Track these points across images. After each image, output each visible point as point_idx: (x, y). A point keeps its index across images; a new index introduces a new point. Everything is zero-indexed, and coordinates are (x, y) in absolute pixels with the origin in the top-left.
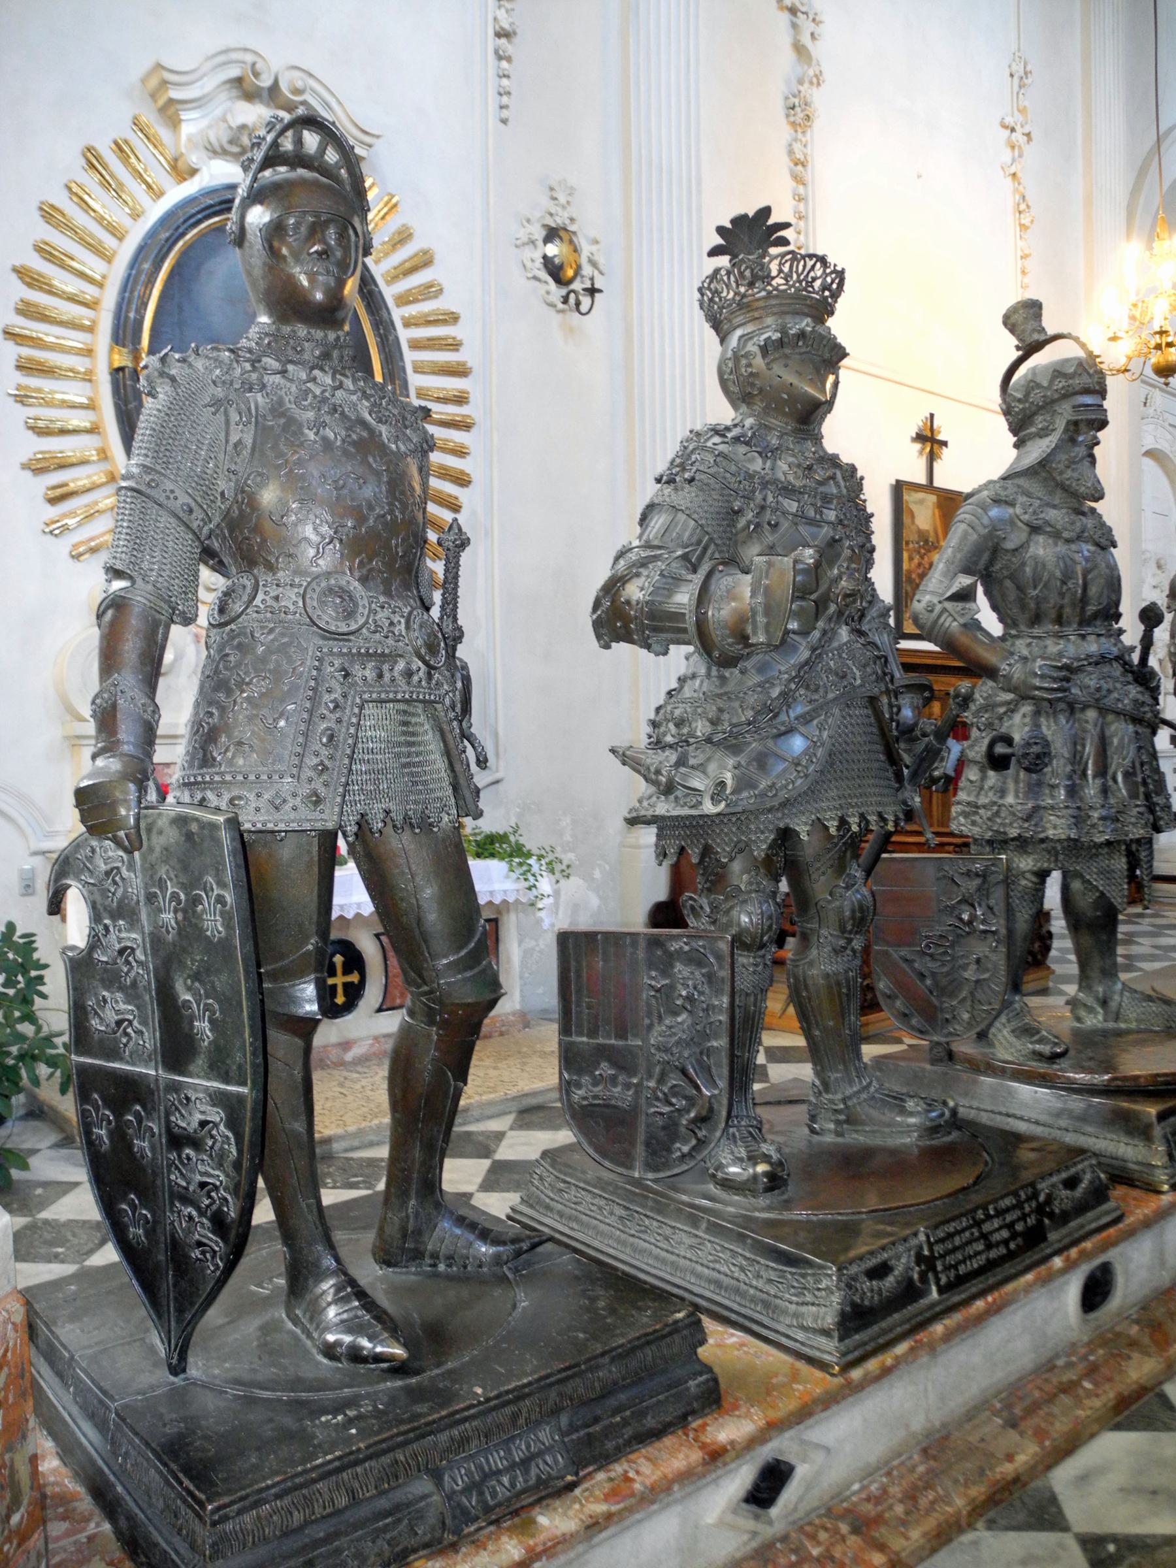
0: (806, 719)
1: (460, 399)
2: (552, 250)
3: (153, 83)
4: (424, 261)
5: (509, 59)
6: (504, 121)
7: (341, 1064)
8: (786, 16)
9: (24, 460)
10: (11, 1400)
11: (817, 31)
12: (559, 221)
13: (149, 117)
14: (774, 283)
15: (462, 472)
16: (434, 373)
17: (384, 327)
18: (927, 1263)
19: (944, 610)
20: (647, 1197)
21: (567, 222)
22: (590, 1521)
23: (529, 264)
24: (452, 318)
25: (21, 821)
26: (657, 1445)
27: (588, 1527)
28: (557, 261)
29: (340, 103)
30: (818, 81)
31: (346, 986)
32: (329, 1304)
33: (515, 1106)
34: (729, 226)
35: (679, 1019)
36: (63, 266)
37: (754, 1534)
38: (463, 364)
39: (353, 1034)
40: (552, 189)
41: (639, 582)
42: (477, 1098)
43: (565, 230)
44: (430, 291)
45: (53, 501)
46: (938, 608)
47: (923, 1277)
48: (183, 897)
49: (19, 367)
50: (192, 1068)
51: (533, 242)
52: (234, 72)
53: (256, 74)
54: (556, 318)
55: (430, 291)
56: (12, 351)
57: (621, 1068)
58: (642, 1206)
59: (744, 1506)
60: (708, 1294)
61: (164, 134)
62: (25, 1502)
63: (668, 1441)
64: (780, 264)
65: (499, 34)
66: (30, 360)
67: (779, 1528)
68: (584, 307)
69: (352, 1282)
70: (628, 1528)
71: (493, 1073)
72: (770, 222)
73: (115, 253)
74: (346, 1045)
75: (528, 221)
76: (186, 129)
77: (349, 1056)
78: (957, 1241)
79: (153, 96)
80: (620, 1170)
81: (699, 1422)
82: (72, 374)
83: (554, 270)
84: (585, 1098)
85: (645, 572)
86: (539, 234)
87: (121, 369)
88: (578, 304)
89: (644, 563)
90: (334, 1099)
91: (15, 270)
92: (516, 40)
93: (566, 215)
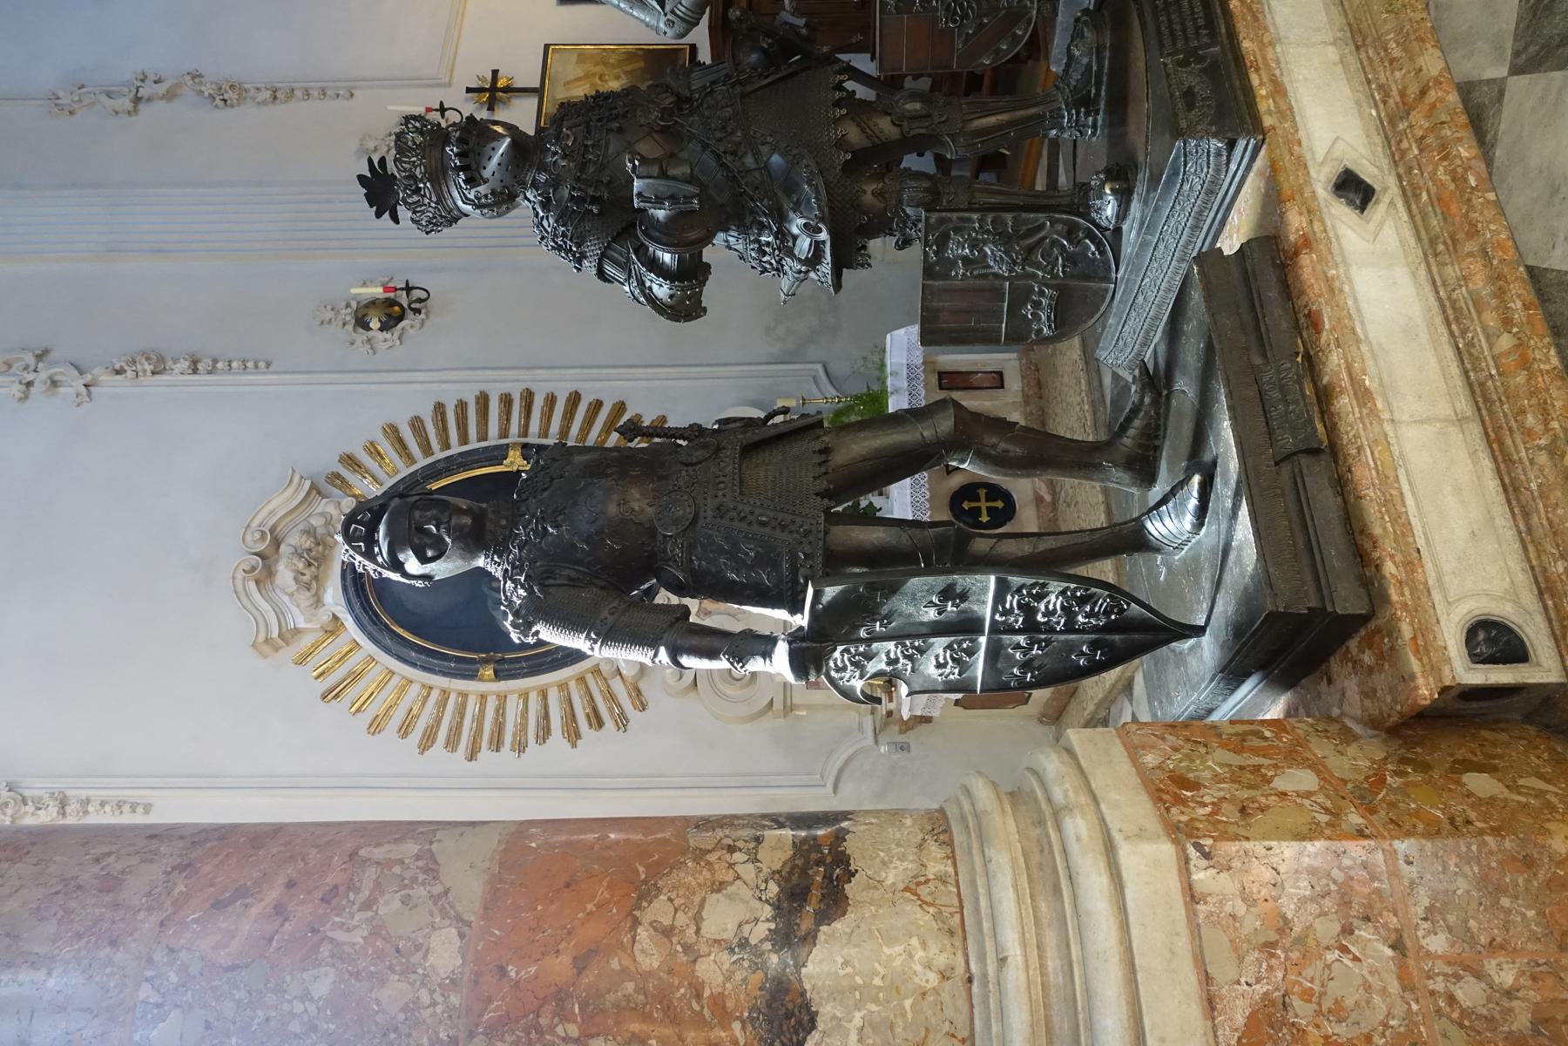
0: (757, 156)
1: (507, 400)
3: (267, 649)
4: (393, 432)
6: (268, 365)
7: (1054, 503)
8: (142, 107)
9: (568, 745)
11: (152, 77)
15: (568, 400)
17: (450, 465)
18: (1192, 56)
19: (673, 12)
24: (439, 408)
25: (851, 751)
30: (196, 76)
37: (1392, 203)
38: (477, 398)
39: (1030, 495)
41: (655, 288)
45: (600, 724)
46: (670, 16)
47: (1201, 59)
49: (498, 750)
52: (252, 586)
53: (253, 569)
55: (417, 425)
56: (485, 754)
57: (1027, 299)
61: (306, 642)
65: (195, 371)
66: (491, 742)
67: (1392, 181)
68: (423, 295)
70: (1359, 311)
71: (1066, 380)
74: (1039, 500)
76: (301, 625)
77: (1048, 498)
78: (1177, 27)
79: (277, 649)
82: (500, 710)
85: (648, 284)
86: (362, 335)
87: (496, 672)
88: (420, 300)
89: (641, 284)
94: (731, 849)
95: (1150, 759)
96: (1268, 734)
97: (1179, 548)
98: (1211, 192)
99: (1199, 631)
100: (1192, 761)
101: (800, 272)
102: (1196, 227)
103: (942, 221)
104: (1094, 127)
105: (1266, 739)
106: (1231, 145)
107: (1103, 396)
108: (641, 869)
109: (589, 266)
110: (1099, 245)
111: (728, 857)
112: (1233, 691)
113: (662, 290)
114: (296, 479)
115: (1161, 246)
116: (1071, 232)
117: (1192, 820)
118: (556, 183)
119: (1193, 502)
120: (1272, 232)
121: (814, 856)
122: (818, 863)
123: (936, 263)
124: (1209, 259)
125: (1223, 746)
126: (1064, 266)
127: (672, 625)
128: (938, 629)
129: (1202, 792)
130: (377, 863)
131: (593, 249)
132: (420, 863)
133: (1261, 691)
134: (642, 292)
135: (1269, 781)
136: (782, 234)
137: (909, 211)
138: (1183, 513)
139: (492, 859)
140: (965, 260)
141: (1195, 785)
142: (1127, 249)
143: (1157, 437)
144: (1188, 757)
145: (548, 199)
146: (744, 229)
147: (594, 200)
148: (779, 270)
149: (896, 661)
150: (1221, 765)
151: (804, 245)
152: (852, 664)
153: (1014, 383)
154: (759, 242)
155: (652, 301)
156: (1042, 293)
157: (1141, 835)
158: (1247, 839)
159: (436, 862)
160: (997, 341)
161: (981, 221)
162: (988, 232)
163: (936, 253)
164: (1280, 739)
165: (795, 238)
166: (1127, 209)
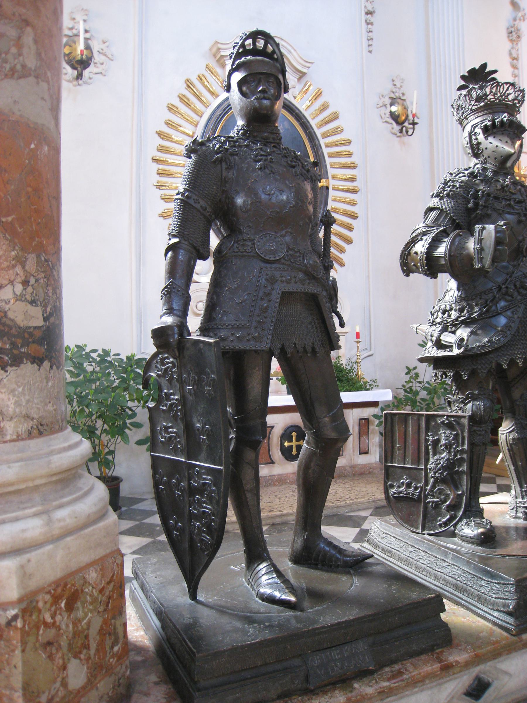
0: (505, 309)
2: (394, 109)
3: (214, 50)
4: (335, 117)
5: (372, 24)
6: (370, 52)
9: (160, 213)
10: (115, 597)
12: (397, 95)
13: (213, 64)
14: (489, 98)
16: (339, 168)
20: (424, 542)
21: (401, 95)
22: (380, 690)
23: (383, 116)
26: (417, 658)
27: (379, 693)
28: (396, 113)
29: (295, 50)
31: (297, 446)
32: (263, 575)
33: (373, 505)
34: (467, 74)
35: (442, 456)
36: (177, 130)
40: (393, 81)
41: (420, 243)
42: (355, 500)
43: (400, 98)
44: (337, 131)
48: (196, 378)
49: (158, 174)
50: (200, 458)
51: (385, 106)
54: (397, 140)
55: (337, 131)
56: (155, 167)
58: (421, 546)
59: (464, 696)
60: (451, 590)
62: (121, 643)
63: (423, 657)
64: (491, 88)
68: (410, 132)
69: (274, 565)
71: (364, 489)
72: (487, 71)
73: (198, 123)
75: (383, 96)
79: (215, 56)
80: (412, 529)
81: (440, 650)
83: (394, 117)
84: (395, 493)
85: (424, 238)
86: (388, 101)
88: (407, 132)
89: (425, 234)
90: (289, 497)
91: (157, 133)
92: (375, 15)
93: (400, 92)
94: (25, 283)
95: (92, 575)
96: (116, 649)
97: (249, 582)
98: (479, 598)
99: (193, 595)
100: (91, 604)
101: (432, 336)
102: (456, 587)
103: (462, 426)
104: (516, 517)
105: (112, 648)
106: (509, 614)
107: (354, 511)
108: (10, 219)
109: (435, 202)
110: (446, 524)
111: (19, 280)
112: (156, 614)
113: (420, 248)
114: (308, 65)
115: (445, 564)
116: (454, 507)
117: (40, 611)
118: (486, 181)
119: (277, 594)
120: (455, 642)
121: (19, 341)
122: (13, 345)
123: (436, 423)
124: (436, 604)
125: (106, 622)
126: (433, 502)
127: (195, 248)
128: (189, 428)
129: (65, 615)
130: (19, 38)
131: (446, 204)
132: (19, 67)
133: (155, 632)
134: (419, 234)
135: (76, 656)
136: (456, 325)
137: (469, 405)
138: (271, 588)
139: (21, 116)
140: (439, 441)
141: (70, 608)
142: (442, 542)
143: (323, 565)
144: (95, 600)
145: (476, 177)
146: (460, 300)
147: (476, 205)
148: (433, 324)
149: (169, 399)
150: (89, 623)
151: (448, 338)
152: (166, 369)
153: (362, 460)
154: (451, 310)
155: (413, 241)
156: (416, 488)
157: (24, 574)
158: (23, 651)
159: (20, 78)
160: (386, 461)
161: (462, 452)
162: (455, 455)
163: (443, 422)
164: (112, 657)
165: (454, 333)
166: (468, 542)
